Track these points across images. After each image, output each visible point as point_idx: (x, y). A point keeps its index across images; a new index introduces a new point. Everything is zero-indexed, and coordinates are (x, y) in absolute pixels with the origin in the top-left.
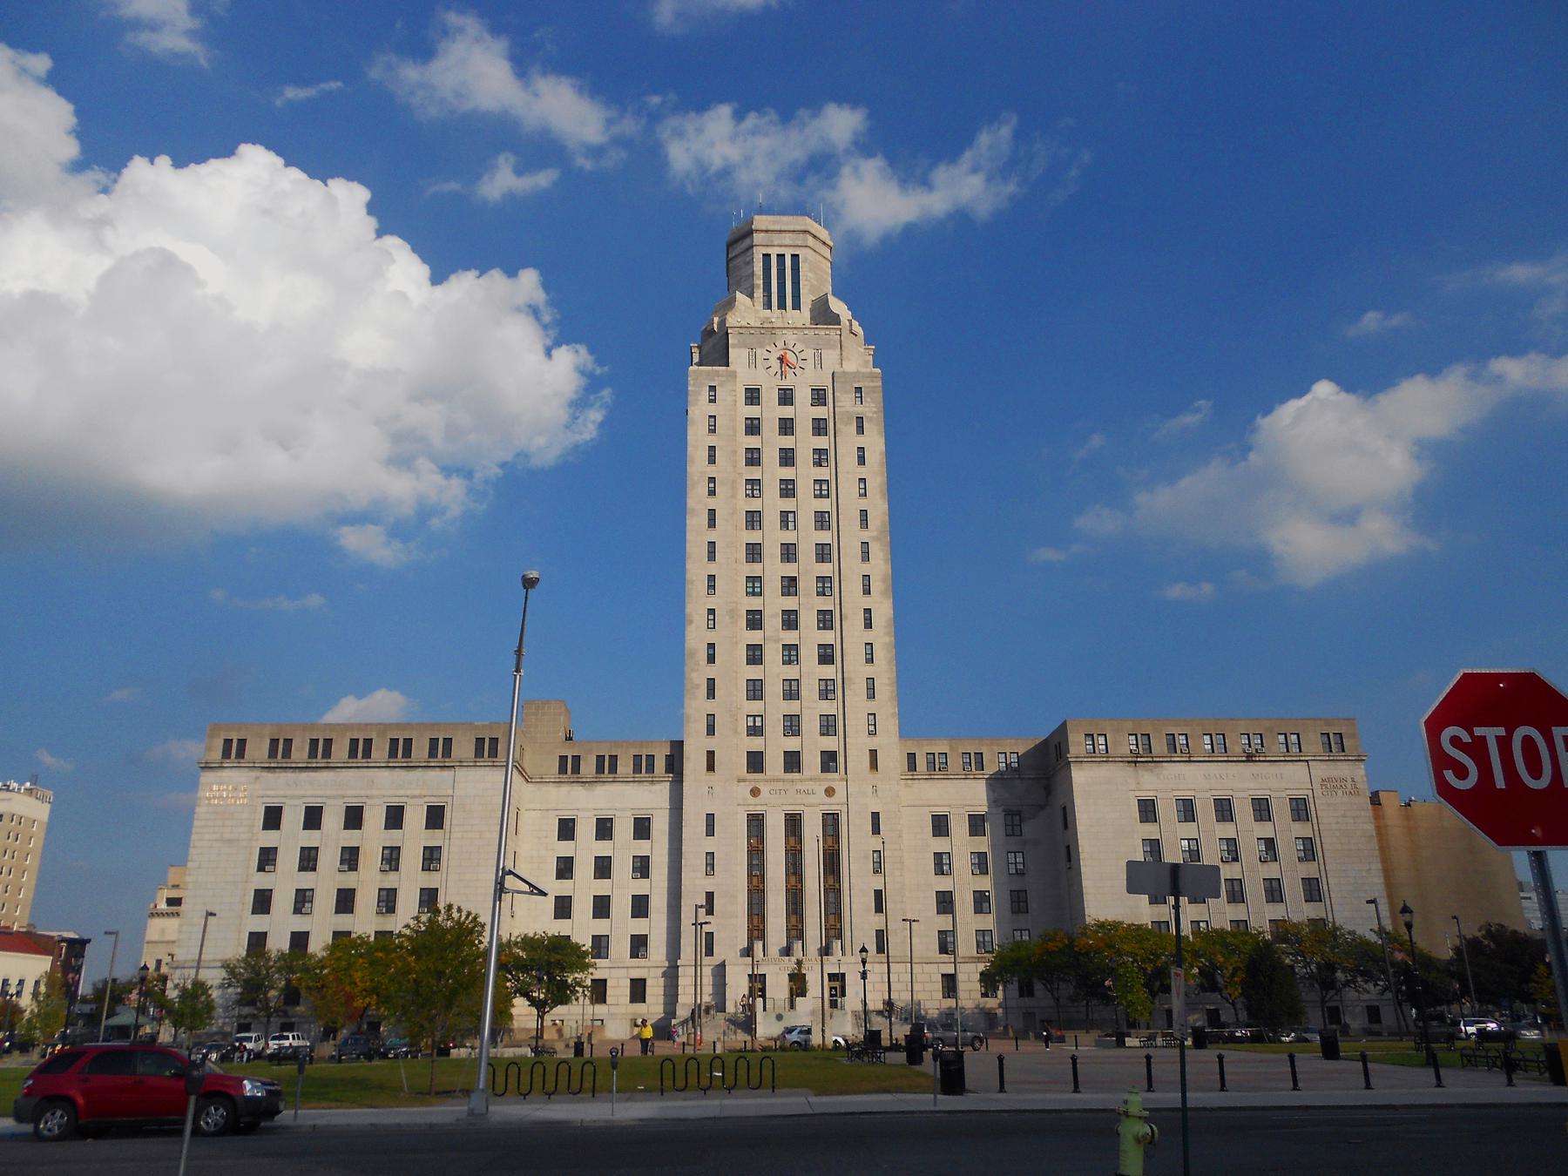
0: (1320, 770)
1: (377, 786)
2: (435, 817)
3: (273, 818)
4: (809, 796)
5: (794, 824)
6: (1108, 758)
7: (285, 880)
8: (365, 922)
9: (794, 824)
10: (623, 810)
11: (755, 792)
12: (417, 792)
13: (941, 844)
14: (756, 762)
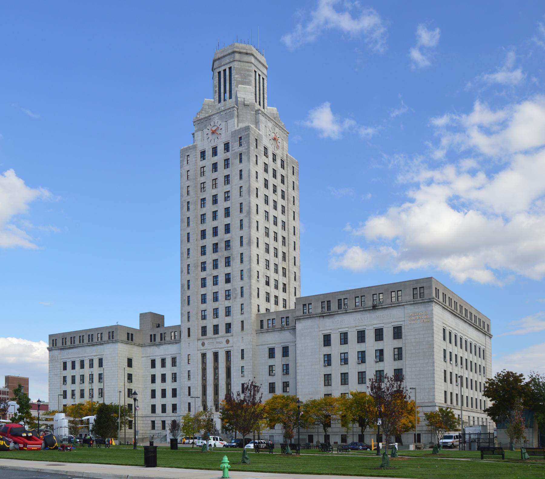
0: (410, 310)
1: (369, 321)
2: (398, 333)
3: (327, 341)
4: (217, 344)
5: (216, 355)
6: (311, 317)
7: (336, 370)
8: (354, 387)
9: (216, 355)
10: (168, 355)
11: (203, 344)
12: (95, 354)
13: (327, 350)
14: (204, 331)
